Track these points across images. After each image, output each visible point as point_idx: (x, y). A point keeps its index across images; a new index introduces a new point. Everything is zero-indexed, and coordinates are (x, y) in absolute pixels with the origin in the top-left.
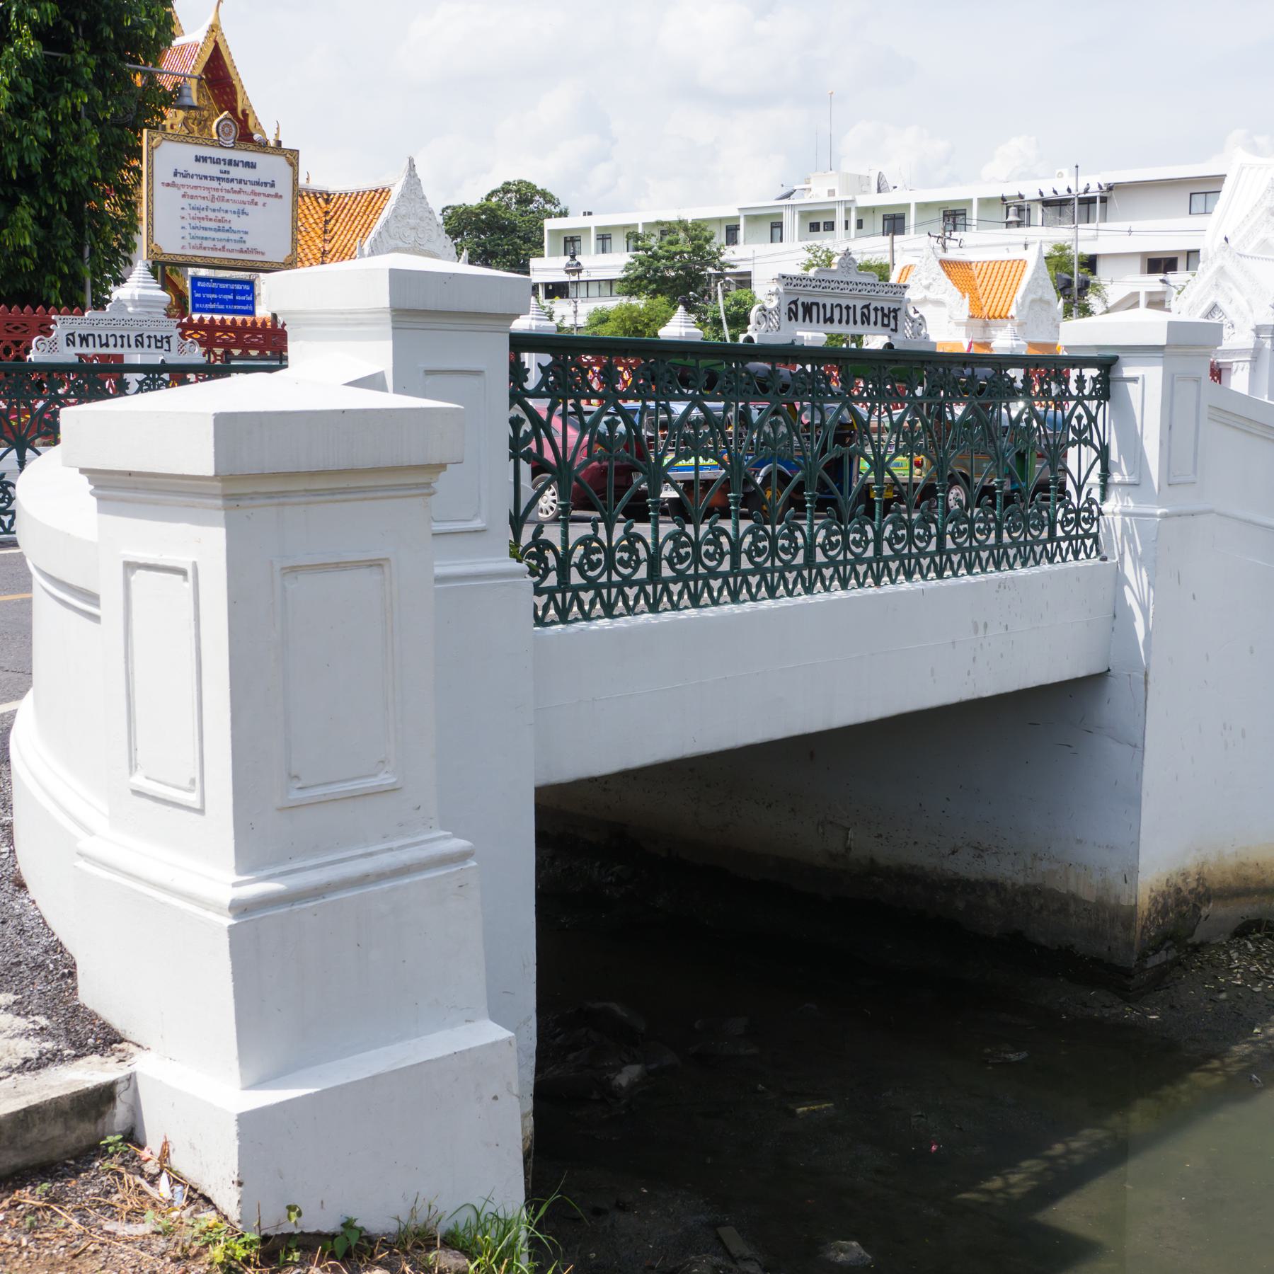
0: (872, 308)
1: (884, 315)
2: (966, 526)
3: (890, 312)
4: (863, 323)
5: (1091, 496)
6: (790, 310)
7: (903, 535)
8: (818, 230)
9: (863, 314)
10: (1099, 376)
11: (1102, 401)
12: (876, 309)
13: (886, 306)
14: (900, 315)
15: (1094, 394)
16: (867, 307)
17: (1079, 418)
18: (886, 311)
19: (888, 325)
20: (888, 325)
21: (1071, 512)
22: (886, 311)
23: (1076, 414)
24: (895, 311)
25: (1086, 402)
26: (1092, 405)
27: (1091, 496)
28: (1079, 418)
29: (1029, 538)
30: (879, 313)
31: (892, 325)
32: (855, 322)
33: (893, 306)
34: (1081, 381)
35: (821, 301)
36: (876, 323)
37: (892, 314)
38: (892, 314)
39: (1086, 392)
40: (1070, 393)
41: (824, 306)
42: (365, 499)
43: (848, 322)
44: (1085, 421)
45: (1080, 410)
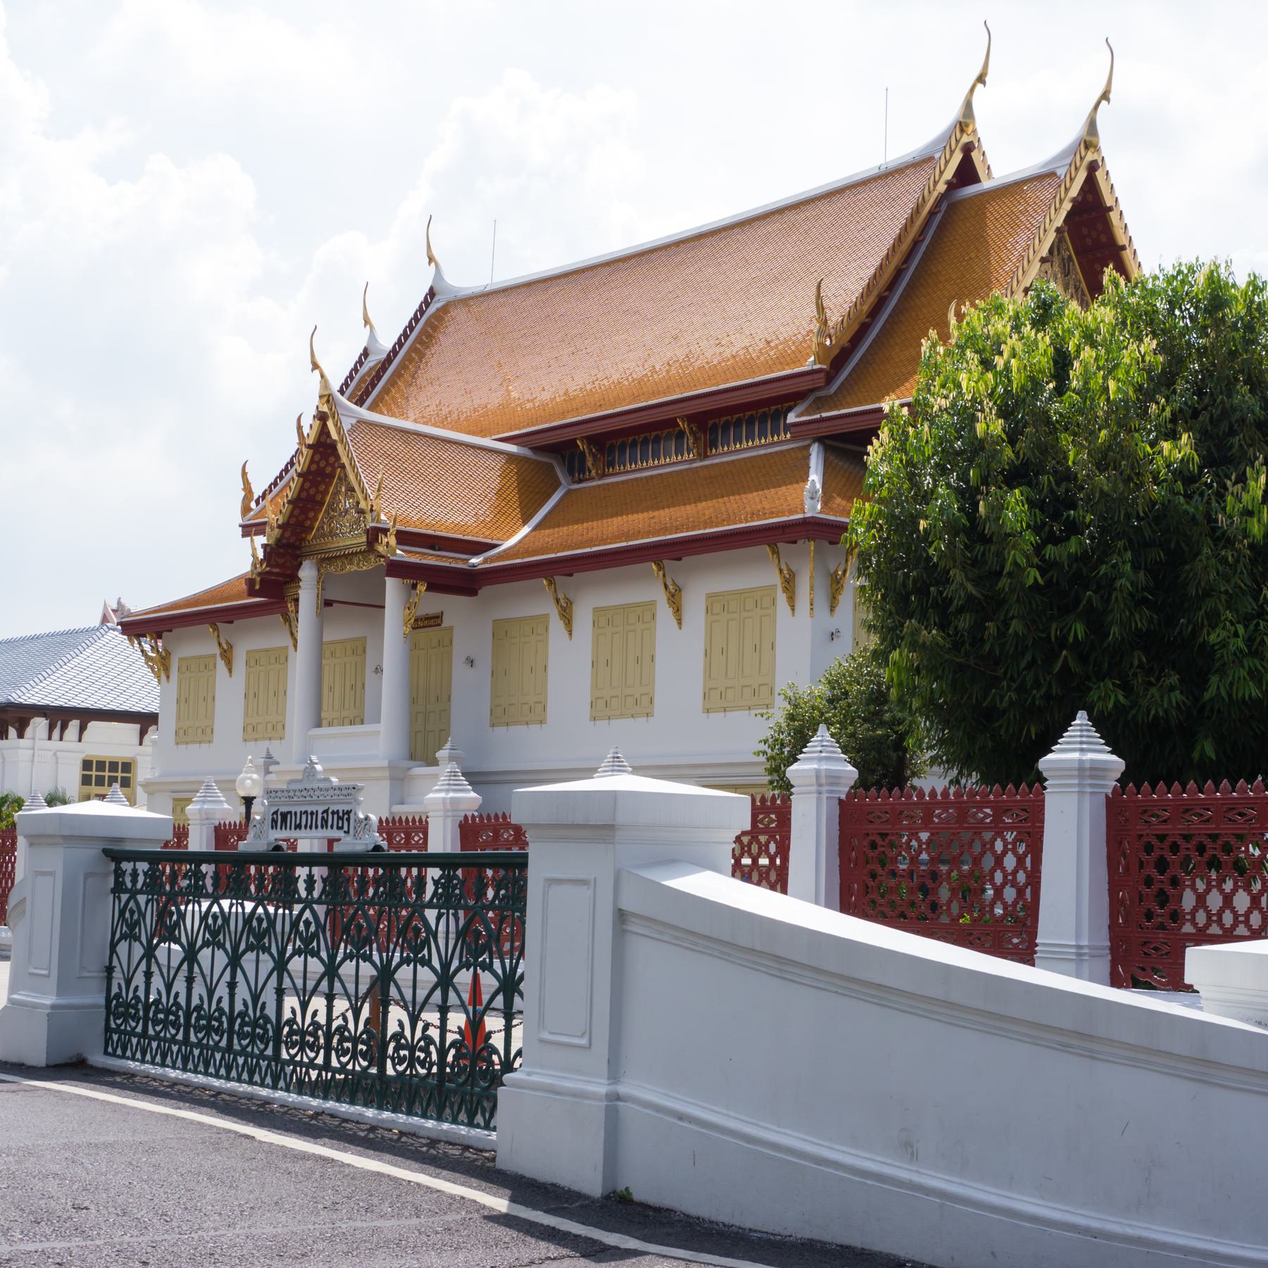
0: (330, 811)
1: (339, 818)
2: (298, 1038)
3: (344, 814)
4: (322, 827)
5: (316, 1019)
6: (273, 819)
7: (405, 1055)
8: (110, 763)
9: (323, 818)
10: (441, 877)
11: (444, 911)
12: (333, 813)
13: (341, 808)
14: (352, 815)
15: (435, 900)
16: (326, 811)
17: (307, 923)
18: (341, 814)
19: (342, 828)
20: (342, 828)
21: (347, 1040)
22: (341, 814)
23: (304, 918)
24: (348, 812)
25: (315, 906)
26: (142, 899)
27: (316, 1019)
28: (307, 923)
29: (168, 1035)
30: (336, 816)
31: (346, 828)
32: (316, 827)
33: (346, 808)
34: (310, 881)
35: (293, 809)
36: (332, 827)
37: (346, 816)
38: (346, 816)
39: (316, 894)
40: (299, 895)
41: (296, 813)
42: (995, 1034)
43: (311, 828)
44: (312, 928)
45: (307, 914)
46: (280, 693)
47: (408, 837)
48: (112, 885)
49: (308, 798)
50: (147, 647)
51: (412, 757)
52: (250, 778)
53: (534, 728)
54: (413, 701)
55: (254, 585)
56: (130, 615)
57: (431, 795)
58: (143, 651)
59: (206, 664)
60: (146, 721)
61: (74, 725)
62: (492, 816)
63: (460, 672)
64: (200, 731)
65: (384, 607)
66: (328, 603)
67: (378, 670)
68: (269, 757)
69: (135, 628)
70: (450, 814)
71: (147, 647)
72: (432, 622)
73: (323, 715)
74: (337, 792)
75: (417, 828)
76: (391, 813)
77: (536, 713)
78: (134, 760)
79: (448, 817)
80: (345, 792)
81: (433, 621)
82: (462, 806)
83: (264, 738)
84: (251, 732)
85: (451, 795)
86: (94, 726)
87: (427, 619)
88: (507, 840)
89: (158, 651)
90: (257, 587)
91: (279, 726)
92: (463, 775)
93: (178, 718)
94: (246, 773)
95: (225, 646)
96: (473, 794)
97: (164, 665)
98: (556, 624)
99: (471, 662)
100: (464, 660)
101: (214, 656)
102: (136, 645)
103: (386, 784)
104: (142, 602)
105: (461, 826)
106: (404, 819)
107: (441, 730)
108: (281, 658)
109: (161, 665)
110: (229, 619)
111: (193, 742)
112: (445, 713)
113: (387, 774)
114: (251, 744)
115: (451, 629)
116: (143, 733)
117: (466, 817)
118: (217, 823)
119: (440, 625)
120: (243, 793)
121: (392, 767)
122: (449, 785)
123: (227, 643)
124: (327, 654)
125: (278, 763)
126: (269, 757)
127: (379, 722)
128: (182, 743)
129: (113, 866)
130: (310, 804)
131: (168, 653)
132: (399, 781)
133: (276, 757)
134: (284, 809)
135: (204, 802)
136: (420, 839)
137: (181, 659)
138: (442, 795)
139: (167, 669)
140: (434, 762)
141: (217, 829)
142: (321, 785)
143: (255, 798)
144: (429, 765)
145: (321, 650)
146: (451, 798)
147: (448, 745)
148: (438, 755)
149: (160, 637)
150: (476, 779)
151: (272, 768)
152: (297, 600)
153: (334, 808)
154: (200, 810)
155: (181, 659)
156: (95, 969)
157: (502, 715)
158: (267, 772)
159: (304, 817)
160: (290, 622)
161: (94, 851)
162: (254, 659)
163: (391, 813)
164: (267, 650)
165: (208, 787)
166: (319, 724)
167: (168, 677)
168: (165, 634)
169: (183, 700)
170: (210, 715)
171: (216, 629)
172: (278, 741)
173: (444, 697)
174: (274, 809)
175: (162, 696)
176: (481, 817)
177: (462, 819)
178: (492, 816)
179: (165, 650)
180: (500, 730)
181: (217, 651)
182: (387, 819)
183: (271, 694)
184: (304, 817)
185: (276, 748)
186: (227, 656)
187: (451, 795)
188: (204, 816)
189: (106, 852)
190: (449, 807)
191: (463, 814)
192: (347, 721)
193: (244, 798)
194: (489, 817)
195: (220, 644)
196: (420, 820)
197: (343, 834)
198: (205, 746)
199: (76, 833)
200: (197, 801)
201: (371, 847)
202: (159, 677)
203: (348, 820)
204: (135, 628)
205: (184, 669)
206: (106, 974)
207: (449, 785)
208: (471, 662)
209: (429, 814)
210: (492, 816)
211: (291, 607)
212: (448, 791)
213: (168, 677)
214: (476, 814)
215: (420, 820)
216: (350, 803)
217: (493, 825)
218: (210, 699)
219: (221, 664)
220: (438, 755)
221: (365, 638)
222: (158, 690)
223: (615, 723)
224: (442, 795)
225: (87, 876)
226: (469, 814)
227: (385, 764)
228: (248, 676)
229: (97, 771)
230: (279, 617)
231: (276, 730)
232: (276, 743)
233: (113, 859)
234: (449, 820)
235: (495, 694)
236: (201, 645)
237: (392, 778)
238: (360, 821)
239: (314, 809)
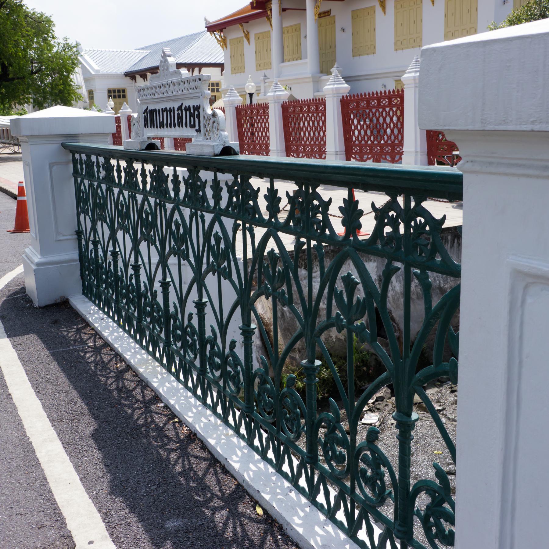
0: (183, 107)
9: (178, 114)
14: (201, 110)
16: (180, 108)
31: (197, 127)
36: (186, 126)
38: (196, 113)
46: (269, 50)
47: (317, 108)
48: (72, 171)
49: (165, 95)
50: (218, 37)
51: (321, 72)
52: (251, 85)
53: (371, 56)
54: (320, 49)
55: (253, 5)
56: (210, 23)
57: (326, 87)
58: (216, 38)
59: (240, 41)
60: (221, 66)
61: (197, 69)
62: (356, 95)
63: (340, 36)
64: (240, 68)
65: (306, 10)
66: (284, 10)
67: (306, 37)
68: (265, 76)
69: (212, 28)
70: (335, 95)
71: (218, 37)
72: (326, 15)
73: (285, 58)
74: (186, 85)
75: (321, 103)
76: (314, 96)
77: (371, 49)
78: (220, 82)
79: (335, 97)
80: (193, 85)
81: (327, 13)
82: (282, 98)
83: (264, 69)
84: (259, 67)
85: (336, 86)
86: (204, 69)
87: (324, 13)
88: (363, 106)
89: (221, 37)
90: (255, 5)
91: (269, 64)
92: (343, 78)
93: (232, 63)
94: (249, 82)
95: (246, 33)
96: (346, 85)
97: (224, 43)
98: (378, 9)
99: (344, 30)
100: (340, 29)
101: (242, 37)
102: (214, 36)
103: (311, 84)
104: (215, 17)
105: (341, 101)
106: (309, 100)
107: (332, 60)
108: (267, 35)
109: (223, 42)
110: (246, 21)
111: (238, 73)
112: (334, 53)
113: (311, 80)
114: (259, 72)
115: (334, 16)
116: (222, 70)
117: (343, 96)
118: (236, 106)
119: (330, 15)
120: (248, 92)
121: (313, 77)
122: (335, 81)
123: (247, 31)
124: (286, 32)
125: (269, 78)
126: (265, 76)
127: (307, 58)
128: (234, 73)
129: (71, 158)
130: (168, 101)
131: (225, 38)
132: (317, 83)
133: (268, 76)
134: (151, 107)
135: (230, 97)
136: (323, 108)
137: (230, 40)
138: (332, 86)
139: (225, 44)
140: (330, 73)
141: (237, 108)
142: (174, 79)
143: (253, 93)
144: (328, 75)
145: (282, 31)
146: (336, 88)
147: (335, 66)
148: (331, 70)
149: (221, 31)
150: (348, 79)
151: (266, 81)
152: (271, 10)
153: (186, 104)
154: (228, 101)
155: (230, 40)
156: (69, 234)
157: (357, 52)
158: (265, 83)
159: (165, 114)
160: (269, 19)
161: (54, 146)
162: (257, 38)
163: (314, 96)
164: (262, 33)
165: (231, 90)
166: (283, 61)
167: (226, 47)
168: (224, 30)
169: (232, 56)
170: (243, 62)
171: (242, 26)
172: (269, 70)
173: (333, 46)
174: (145, 108)
175: (225, 55)
176: (350, 96)
177: (341, 97)
178: (356, 95)
179: (224, 36)
180: (357, 58)
181: (243, 35)
182: (313, 99)
183: (265, 51)
184: (165, 114)
185: (268, 72)
186: (247, 36)
187: (336, 86)
188: (230, 103)
189: (63, 145)
190: (335, 92)
191: (342, 95)
192: (295, 59)
193: (249, 94)
194: (354, 96)
195: (244, 32)
196: (322, 99)
197: (195, 133)
198: (242, 74)
199: (36, 133)
200: (227, 97)
201: (218, 150)
202: (223, 48)
203: (199, 116)
204: (212, 28)
205: (232, 44)
206: (76, 236)
207: (335, 81)
208: (344, 30)
209: (326, 96)
210: (363, 94)
211: (269, 13)
212: (334, 84)
213: (226, 47)
214: (348, 95)
215: (322, 99)
216: (198, 97)
217: (356, 100)
218: (242, 55)
219: (245, 40)
220: (331, 70)
221: (300, 24)
222: (223, 53)
223: (405, 51)
224: (332, 86)
225: (51, 165)
226: (345, 95)
227: (310, 75)
228: (256, 44)
229: (216, 86)
230: (265, 18)
231: (268, 66)
232: (268, 71)
233: (71, 151)
234: (335, 98)
235: (354, 43)
236: (236, 33)
237: (314, 82)
238: (208, 119)
239: (169, 105)
